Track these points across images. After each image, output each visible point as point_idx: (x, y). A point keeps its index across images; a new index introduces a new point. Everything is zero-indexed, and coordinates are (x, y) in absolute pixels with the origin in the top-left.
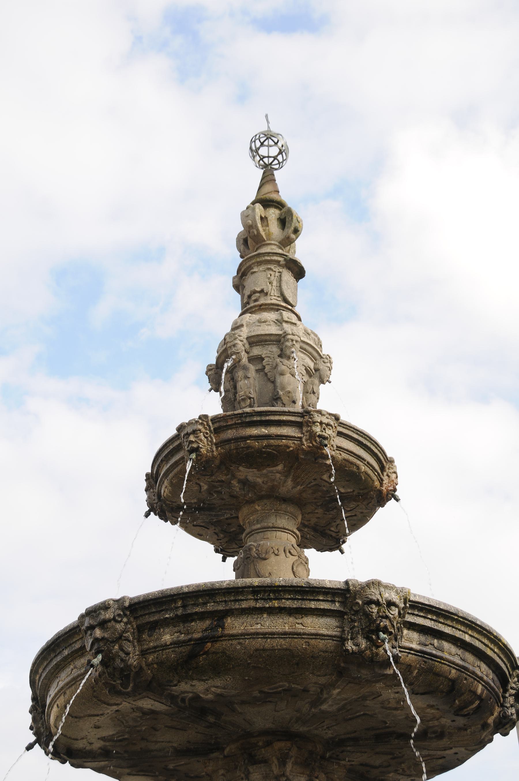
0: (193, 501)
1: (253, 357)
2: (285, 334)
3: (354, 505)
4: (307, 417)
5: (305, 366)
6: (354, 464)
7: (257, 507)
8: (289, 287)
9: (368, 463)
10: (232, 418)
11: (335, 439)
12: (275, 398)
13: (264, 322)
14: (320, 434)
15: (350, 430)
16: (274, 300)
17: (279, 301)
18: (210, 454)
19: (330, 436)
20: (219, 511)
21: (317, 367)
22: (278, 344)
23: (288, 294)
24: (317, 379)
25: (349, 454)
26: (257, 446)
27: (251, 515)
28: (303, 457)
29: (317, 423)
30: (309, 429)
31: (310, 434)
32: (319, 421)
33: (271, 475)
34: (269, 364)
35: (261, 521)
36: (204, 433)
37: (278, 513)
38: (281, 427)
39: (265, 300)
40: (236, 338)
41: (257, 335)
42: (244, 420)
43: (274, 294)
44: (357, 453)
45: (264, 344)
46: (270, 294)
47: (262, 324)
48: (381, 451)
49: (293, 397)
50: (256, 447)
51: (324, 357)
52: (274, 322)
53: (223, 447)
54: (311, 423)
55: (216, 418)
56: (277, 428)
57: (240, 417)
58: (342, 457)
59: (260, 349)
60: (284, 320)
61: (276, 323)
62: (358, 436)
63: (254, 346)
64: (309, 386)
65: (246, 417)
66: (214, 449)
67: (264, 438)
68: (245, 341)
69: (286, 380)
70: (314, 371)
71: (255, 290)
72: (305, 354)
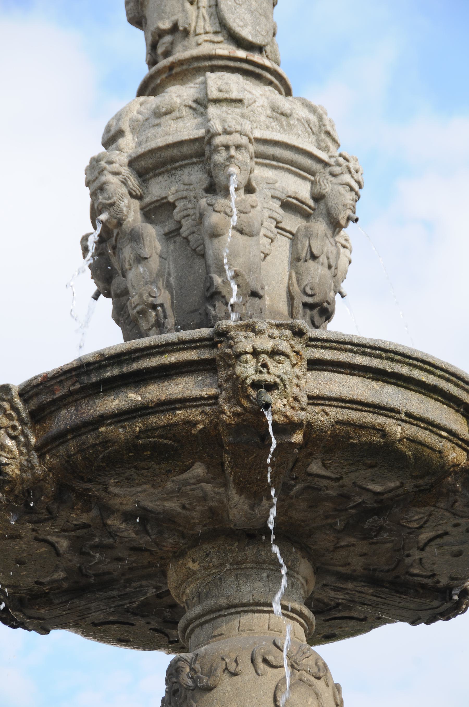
0: (56, 576)
2: (209, 135)
3: (420, 513)
5: (279, 199)
6: (369, 425)
7: (190, 565)
9: (408, 415)
10: (61, 382)
12: (208, 294)
13: (166, 114)
14: (254, 381)
15: (341, 350)
17: (218, 43)
18: (27, 475)
19: (282, 380)
20: (125, 587)
21: (317, 190)
22: (202, 162)
23: (238, 21)
26: (122, 436)
27: (184, 585)
28: (231, 439)
30: (229, 373)
33: (192, 490)
34: (188, 215)
35: (207, 594)
36: (6, 428)
37: (239, 569)
38: (170, 379)
39: (186, 48)
42: (86, 382)
43: (204, 28)
44: (371, 398)
46: (195, 30)
47: (163, 119)
48: (447, 375)
50: (121, 439)
52: (190, 107)
53: (54, 452)
54: (233, 359)
55: (28, 388)
56: (161, 385)
57: (78, 376)
59: (164, 183)
62: (368, 358)
63: (151, 178)
66: (36, 461)
67: (134, 415)
68: (125, 171)
71: (158, 28)
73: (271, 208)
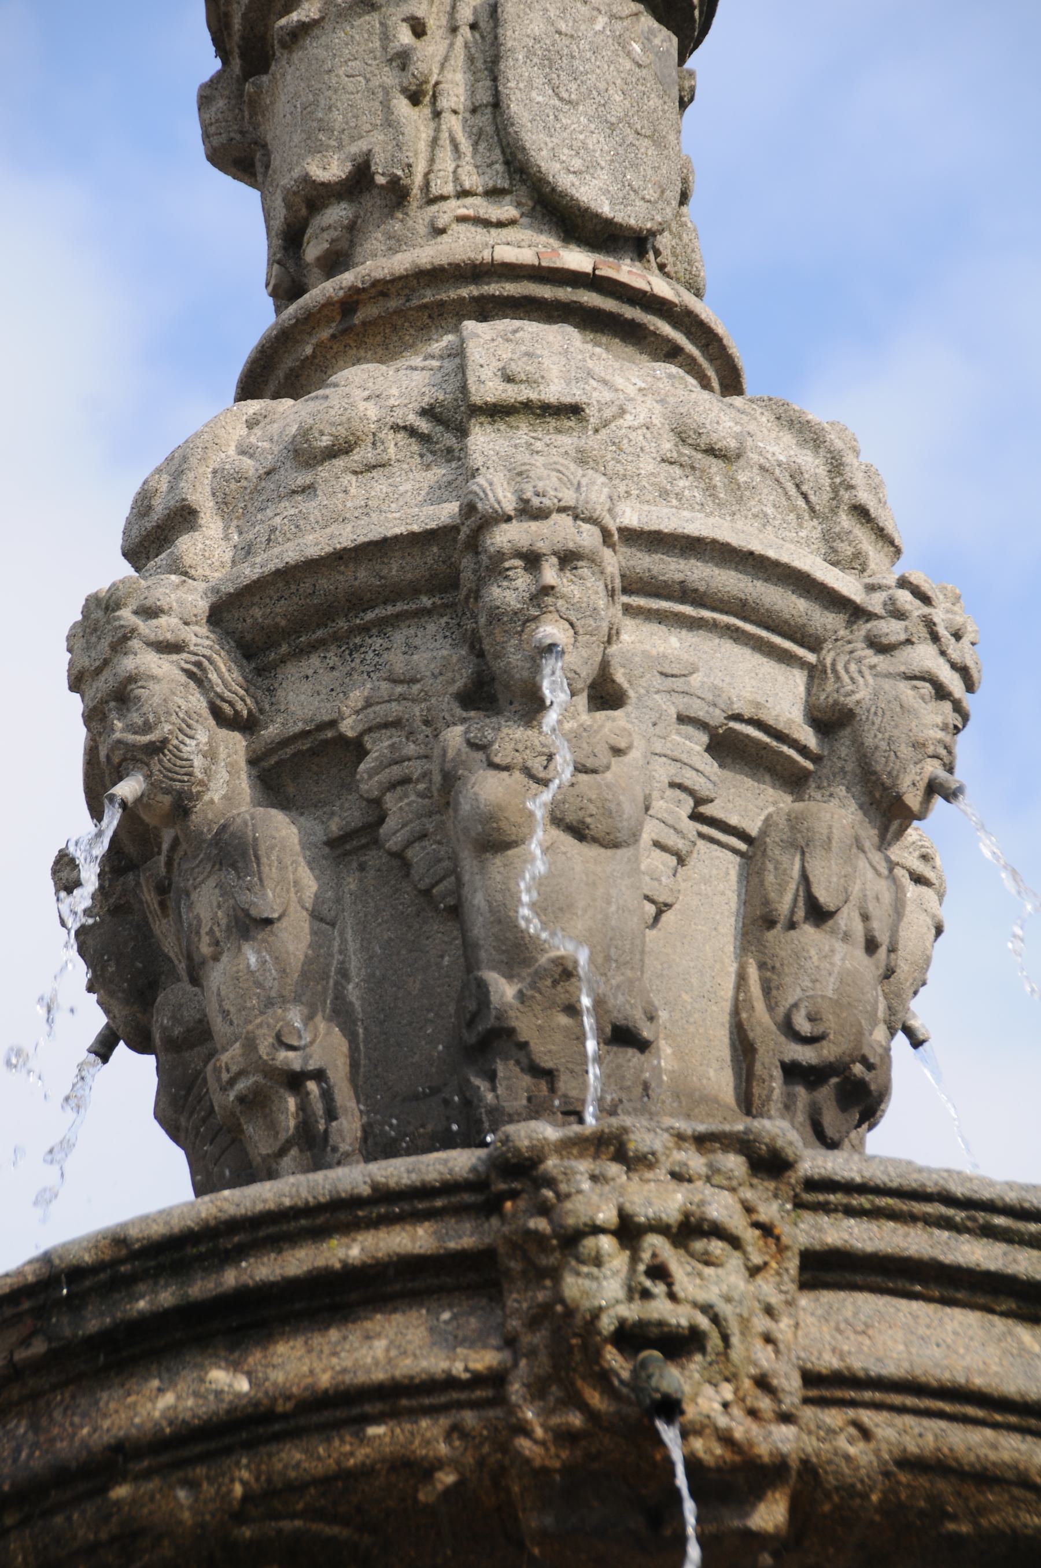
1: (290, 750)
4: (522, 1204)
5: (701, 725)
6: (1010, 1475)
8: (571, 89)
13: (332, 453)
14: (622, 1322)
15: (911, 1219)
16: (462, 227)
17: (500, 224)
19: (715, 1319)
23: (565, 153)
25: (941, 1415)
31: (558, 1338)
32: (607, 1215)
34: (406, 781)
39: (396, 245)
40: (126, 639)
41: (278, 573)
42: (67, 1332)
43: (456, 179)
46: (427, 184)
47: (324, 471)
50: (180, 1522)
51: (875, 603)
52: (412, 431)
54: (553, 1249)
57: (41, 1312)
58: (877, 1453)
59: (327, 679)
62: (999, 1248)
63: (283, 661)
64: (777, 864)
65: (74, 1304)
70: (808, 737)
72: (694, 624)
73: (676, 754)
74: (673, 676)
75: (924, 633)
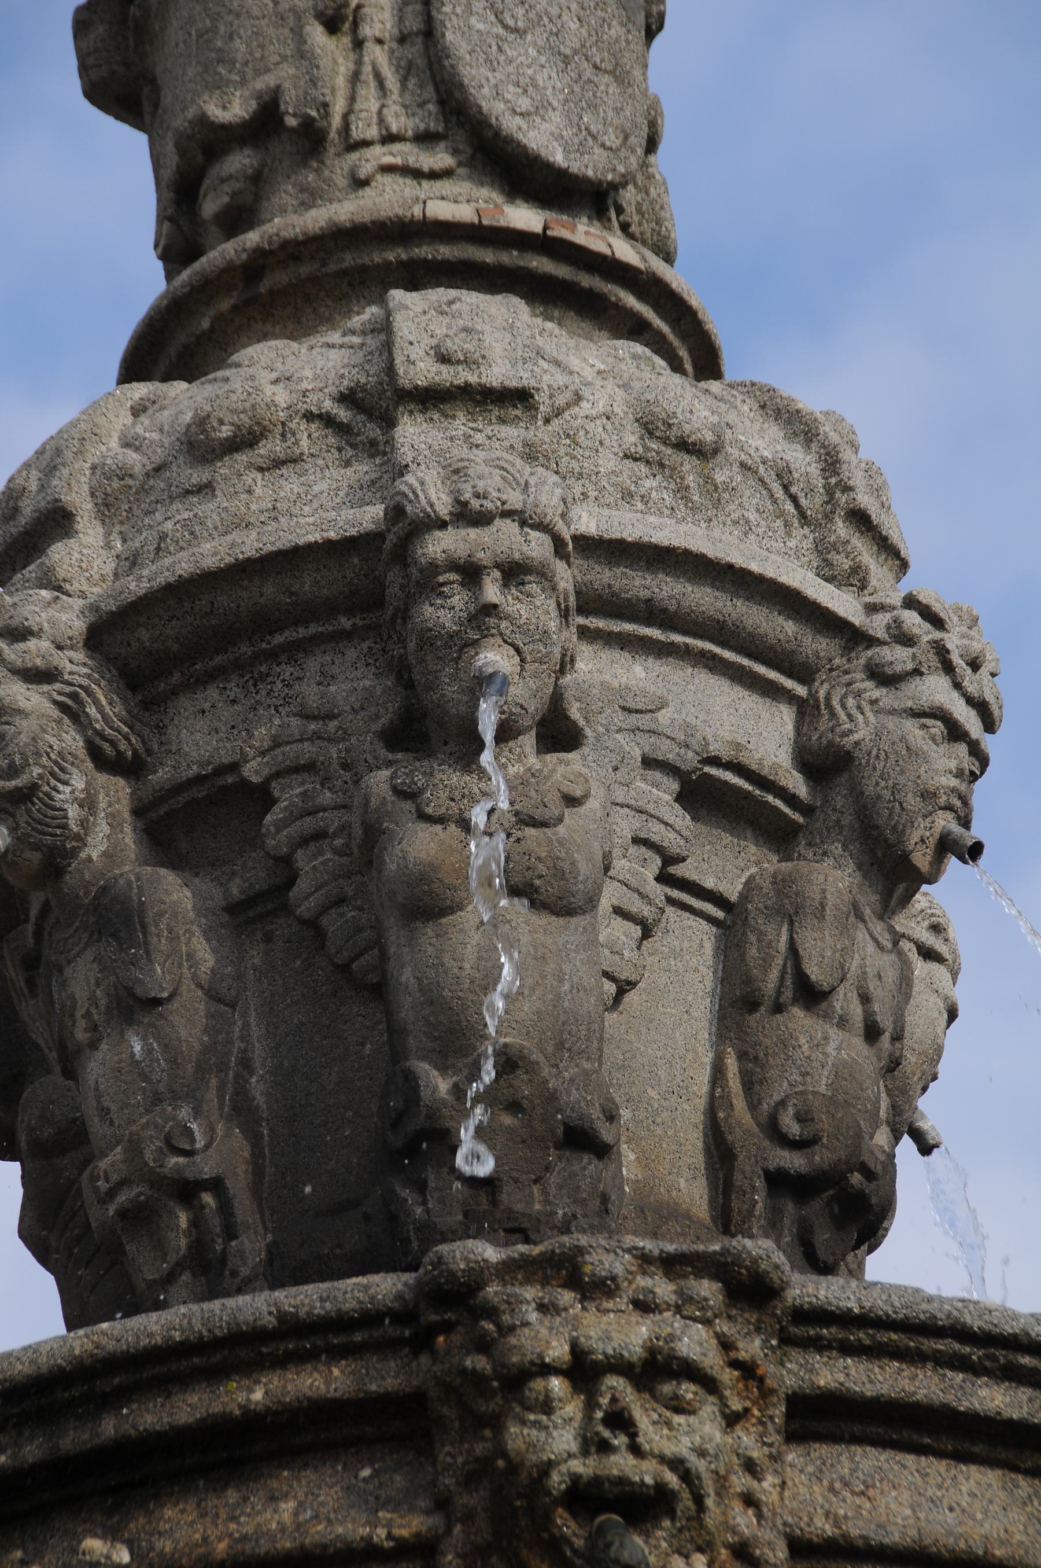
1: (182, 799)
2: (400, 528)
11: (769, 1481)
16: (387, 181)
19: (687, 1476)
23: (510, 92)
24: (837, 848)
29: (538, 1384)
32: (558, 1351)
34: (320, 835)
39: (310, 198)
43: (381, 121)
45: (259, 657)
47: (224, 468)
49: (552, 1098)
51: (878, 625)
59: (226, 713)
60: (404, 382)
61: (342, 429)
63: (175, 692)
69: (470, 953)
74: (637, 711)
75: (934, 661)
